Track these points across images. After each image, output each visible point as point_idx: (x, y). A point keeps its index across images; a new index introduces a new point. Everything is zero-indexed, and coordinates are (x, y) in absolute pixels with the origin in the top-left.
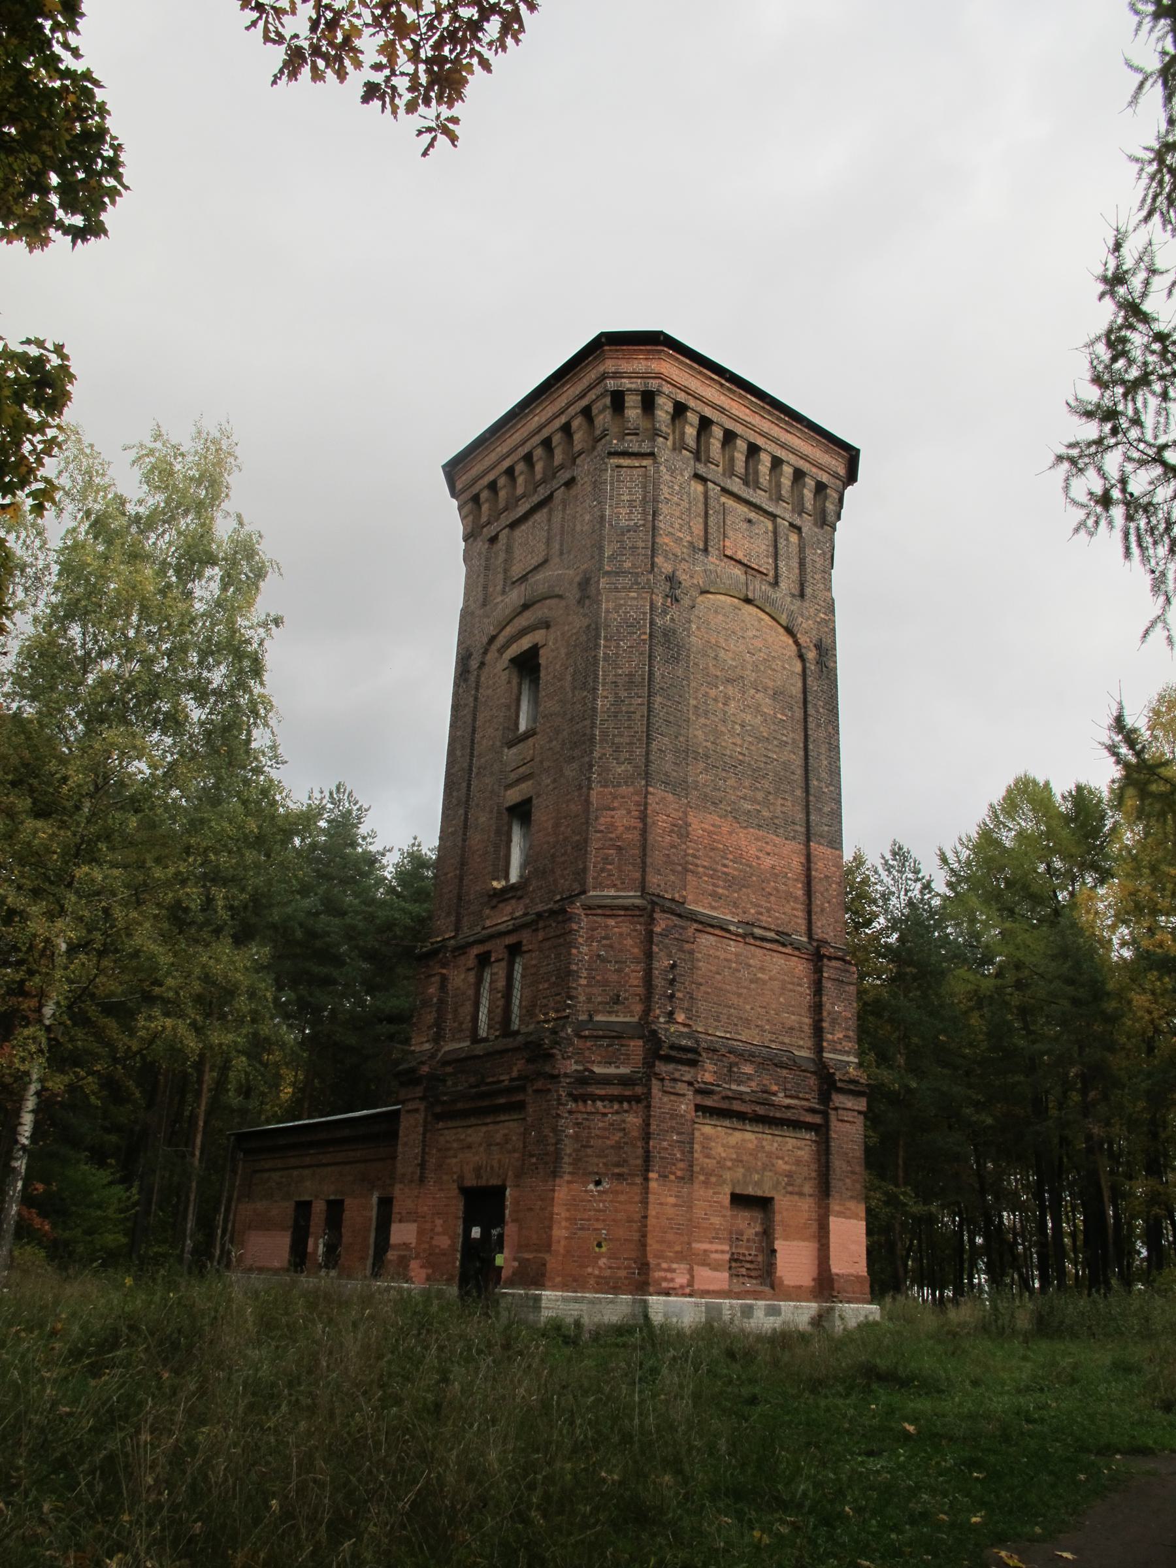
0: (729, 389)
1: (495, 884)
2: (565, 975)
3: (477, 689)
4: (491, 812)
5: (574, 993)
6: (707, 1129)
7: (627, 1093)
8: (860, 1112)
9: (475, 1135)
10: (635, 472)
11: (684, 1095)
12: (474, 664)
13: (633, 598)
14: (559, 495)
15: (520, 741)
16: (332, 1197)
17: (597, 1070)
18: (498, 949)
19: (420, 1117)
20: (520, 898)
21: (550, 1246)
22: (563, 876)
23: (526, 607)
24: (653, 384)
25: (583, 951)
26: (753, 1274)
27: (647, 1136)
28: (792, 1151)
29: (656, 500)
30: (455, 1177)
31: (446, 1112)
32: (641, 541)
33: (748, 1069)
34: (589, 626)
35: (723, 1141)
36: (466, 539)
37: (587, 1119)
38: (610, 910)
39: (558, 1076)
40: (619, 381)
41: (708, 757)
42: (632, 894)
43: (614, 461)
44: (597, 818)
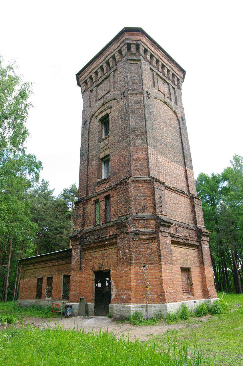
0: (157, 49)
1: (98, 180)
2: (127, 201)
3: (89, 129)
4: (96, 160)
5: (131, 206)
6: (174, 248)
7: (151, 237)
8: (208, 241)
9: (98, 254)
10: (135, 65)
11: (168, 237)
12: (88, 123)
13: (138, 96)
14: (112, 74)
15: (104, 140)
16: (49, 276)
17: (141, 230)
18: (102, 197)
19: (79, 250)
20: (108, 182)
21: (131, 289)
22: (123, 173)
23: (103, 104)
24: (139, 42)
25: (132, 193)
26: (187, 292)
27: (159, 250)
28: (192, 253)
29: (141, 72)
30: (91, 268)
31: (85, 248)
32: (138, 82)
33: (180, 229)
34: (125, 104)
35: (178, 251)
36: (82, 93)
37: (139, 246)
38: (140, 181)
39: (129, 232)
40: (129, 41)
41: (160, 141)
42: (146, 176)
43: (129, 62)
44: (133, 155)
